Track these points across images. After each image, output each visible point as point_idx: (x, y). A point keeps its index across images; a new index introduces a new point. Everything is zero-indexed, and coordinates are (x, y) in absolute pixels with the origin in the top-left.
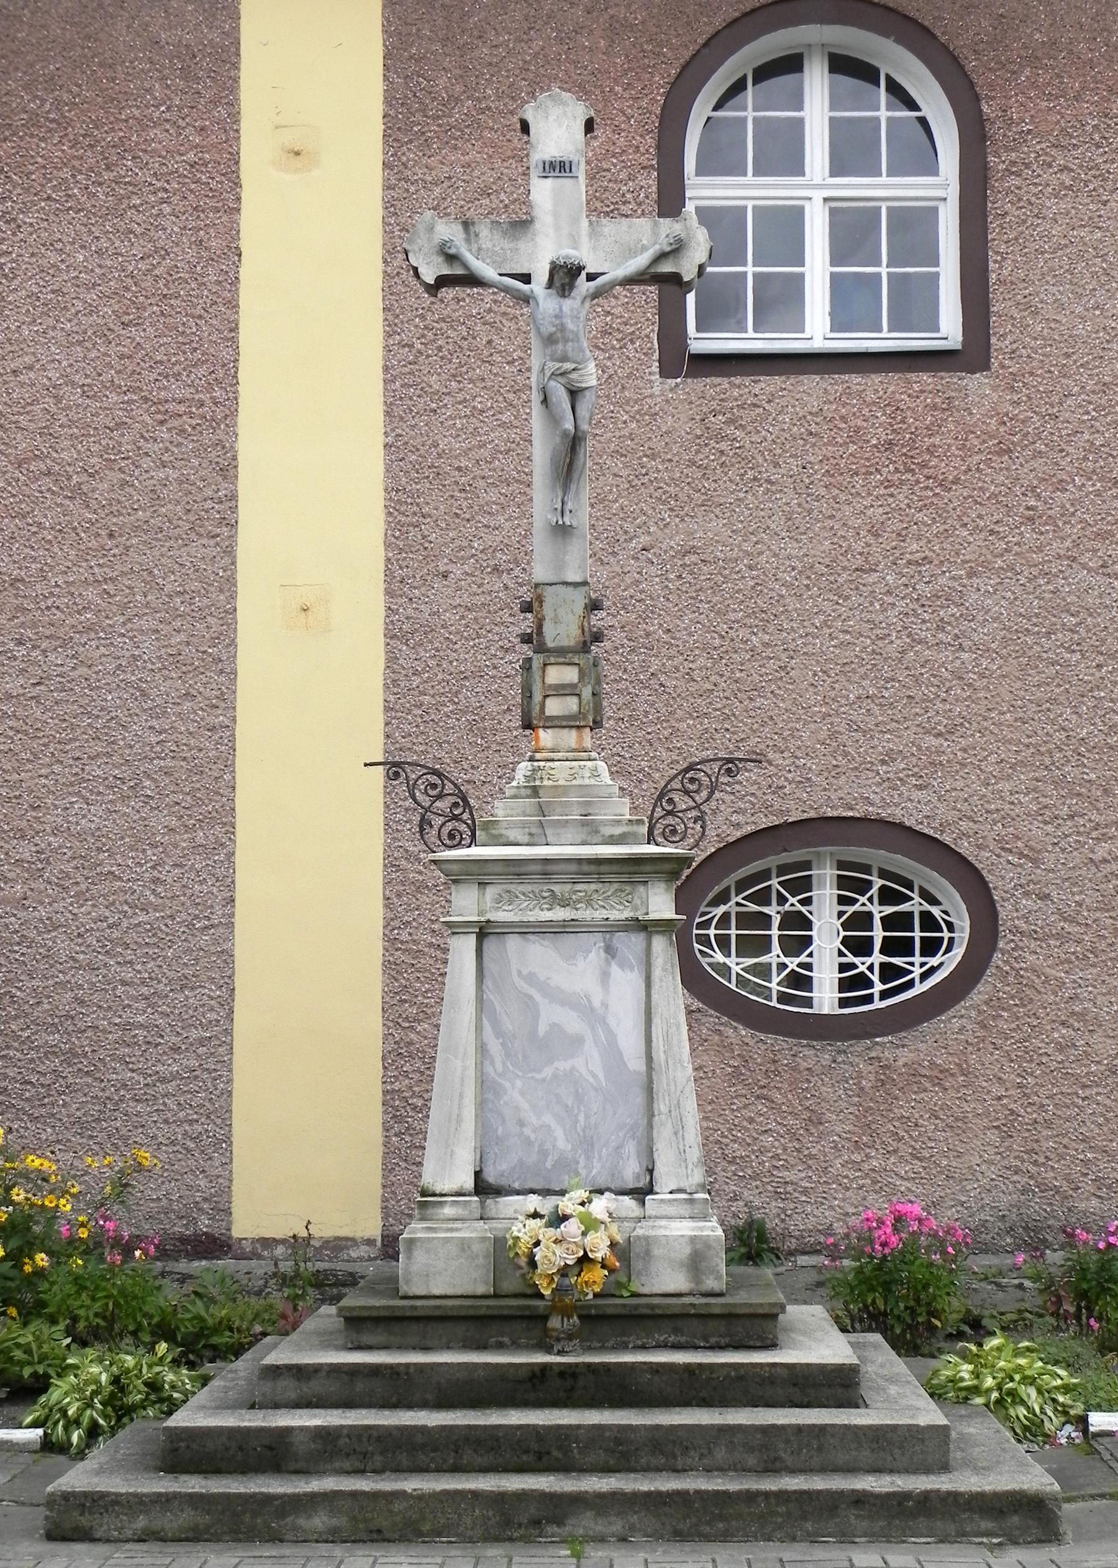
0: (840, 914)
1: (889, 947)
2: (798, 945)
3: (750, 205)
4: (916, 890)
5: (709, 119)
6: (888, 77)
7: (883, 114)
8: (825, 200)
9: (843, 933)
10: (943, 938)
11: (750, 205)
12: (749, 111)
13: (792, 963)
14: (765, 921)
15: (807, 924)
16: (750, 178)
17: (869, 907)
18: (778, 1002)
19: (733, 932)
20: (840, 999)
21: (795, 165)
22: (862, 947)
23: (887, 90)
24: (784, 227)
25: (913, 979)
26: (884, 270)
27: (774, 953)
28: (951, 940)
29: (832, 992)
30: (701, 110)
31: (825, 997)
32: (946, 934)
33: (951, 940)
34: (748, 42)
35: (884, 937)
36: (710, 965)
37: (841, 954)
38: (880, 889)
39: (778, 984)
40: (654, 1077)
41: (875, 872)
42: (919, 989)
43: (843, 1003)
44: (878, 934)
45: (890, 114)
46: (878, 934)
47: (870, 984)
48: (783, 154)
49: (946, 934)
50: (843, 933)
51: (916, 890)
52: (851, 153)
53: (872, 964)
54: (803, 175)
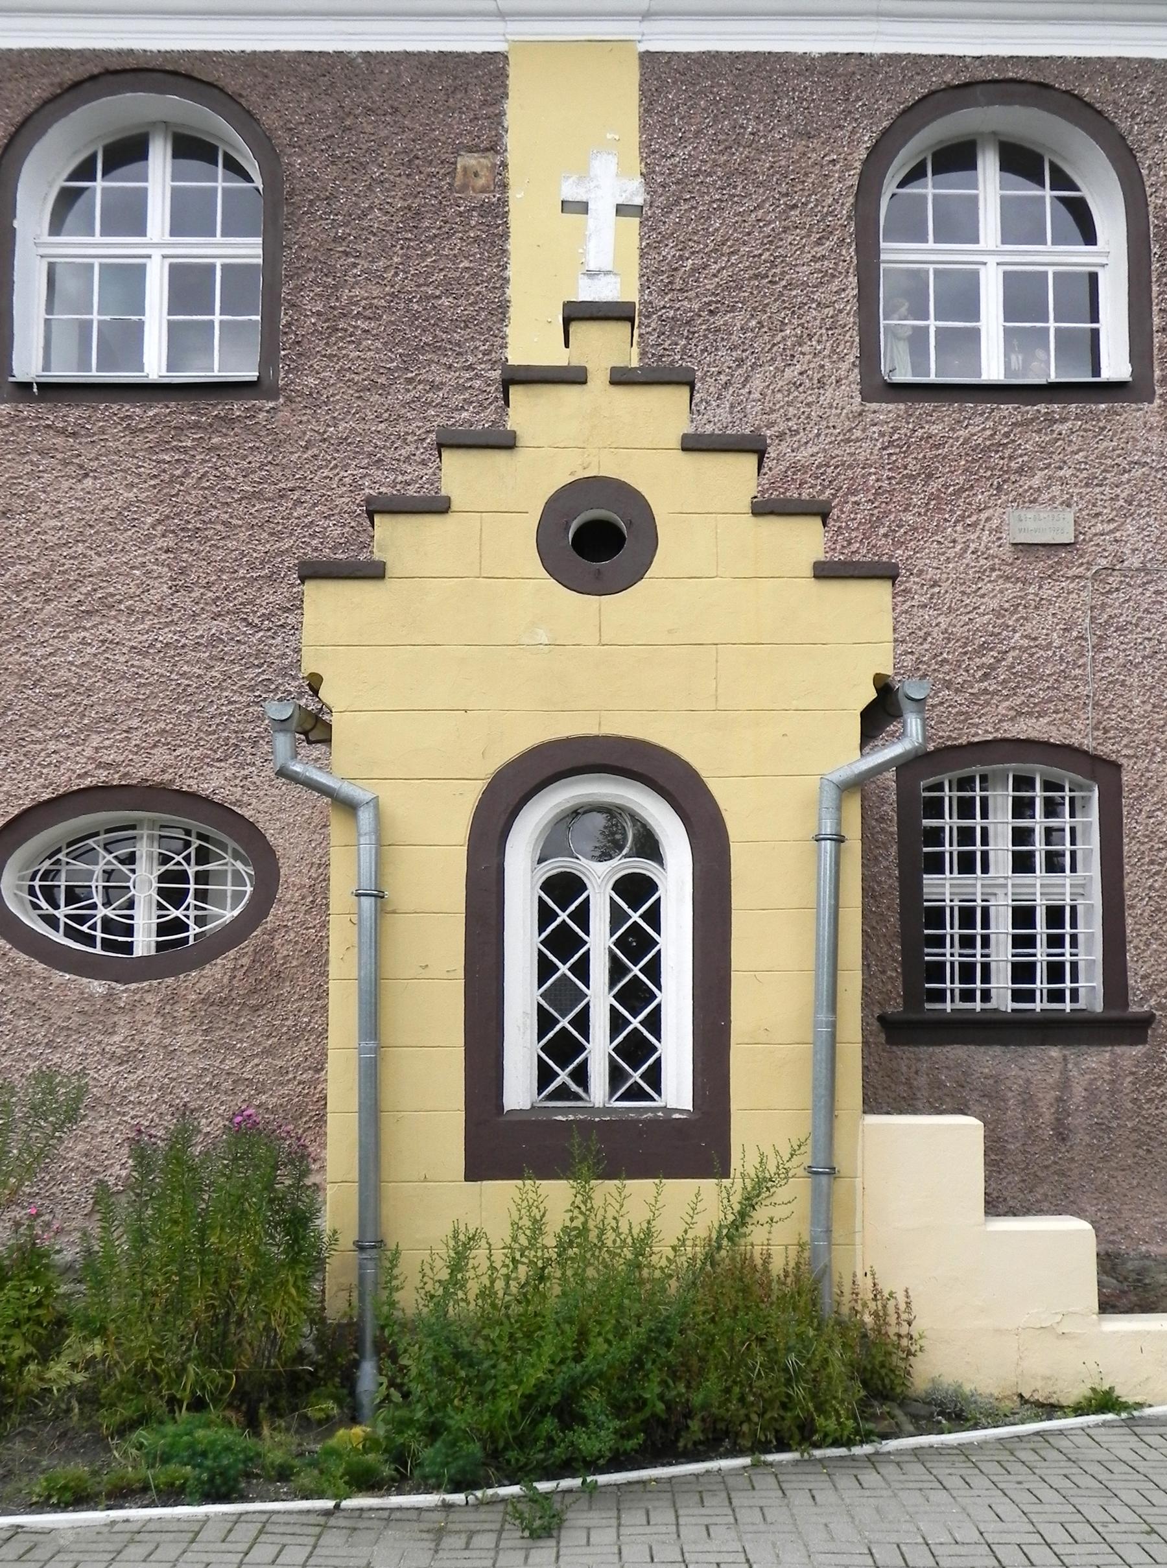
3: (1051, 270)
4: (230, 851)
5: (893, 195)
6: (1052, 164)
7: (220, 185)
11: (1051, 270)
12: (929, 189)
14: (183, 877)
16: (98, 238)
17: (102, 863)
18: (103, 949)
20: (157, 942)
21: (139, 228)
22: (176, 898)
23: (225, 166)
24: (128, 278)
26: (1052, 325)
30: (890, 187)
31: (144, 942)
37: (160, 906)
38: (197, 849)
40: (824, 1017)
41: (194, 834)
43: (160, 946)
47: (186, 928)
48: (959, 225)
49: (37, 883)
51: (230, 851)
52: (188, 218)
54: (1095, 244)
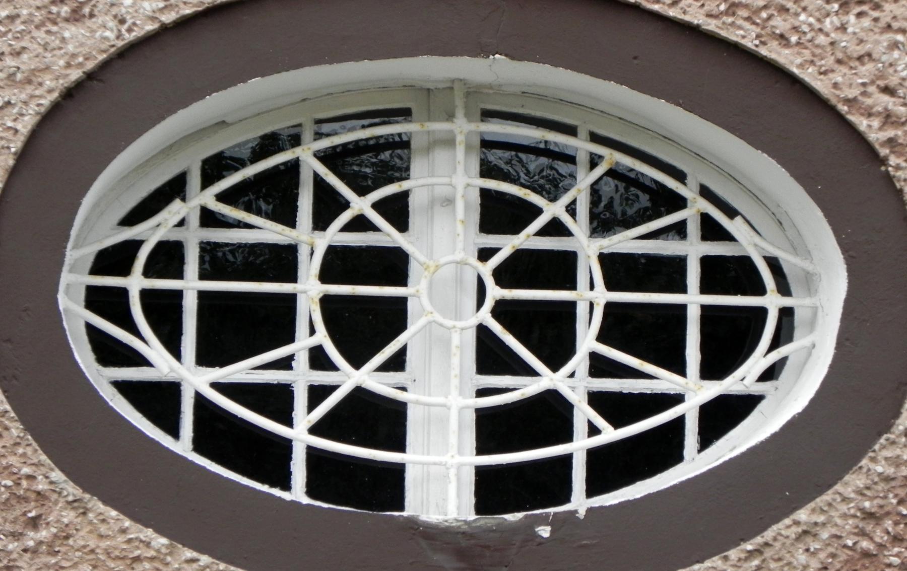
0: (485, 254)
1: (618, 325)
2: (367, 327)
8: (487, 144)
9: (495, 292)
10: (762, 313)
13: (348, 378)
15: (393, 266)
19: (191, 285)
22: (551, 334)
25: (680, 422)
27: (302, 344)
28: (786, 313)
29: (460, 452)
32: (772, 302)
33: (786, 313)
34: (762, 443)
35: (610, 307)
36: (124, 387)
39: (316, 430)
42: (695, 463)
44: (591, 296)
45: (190, 305)
46: (591, 296)
50: (495, 292)
53: (569, 234)
